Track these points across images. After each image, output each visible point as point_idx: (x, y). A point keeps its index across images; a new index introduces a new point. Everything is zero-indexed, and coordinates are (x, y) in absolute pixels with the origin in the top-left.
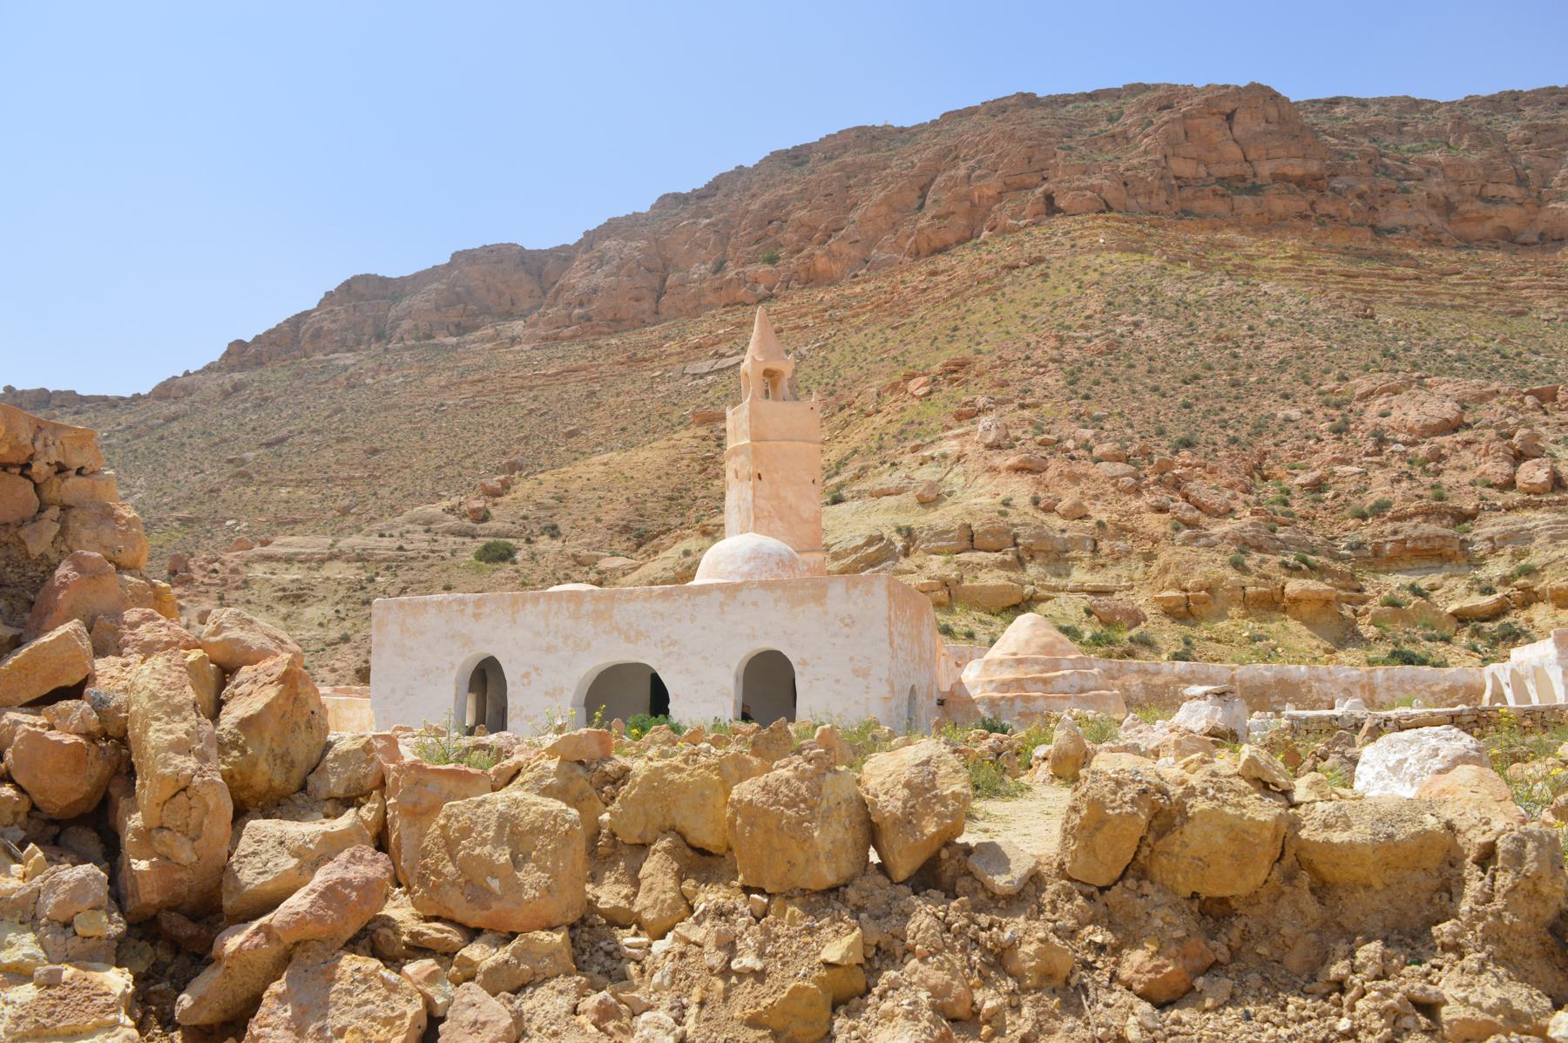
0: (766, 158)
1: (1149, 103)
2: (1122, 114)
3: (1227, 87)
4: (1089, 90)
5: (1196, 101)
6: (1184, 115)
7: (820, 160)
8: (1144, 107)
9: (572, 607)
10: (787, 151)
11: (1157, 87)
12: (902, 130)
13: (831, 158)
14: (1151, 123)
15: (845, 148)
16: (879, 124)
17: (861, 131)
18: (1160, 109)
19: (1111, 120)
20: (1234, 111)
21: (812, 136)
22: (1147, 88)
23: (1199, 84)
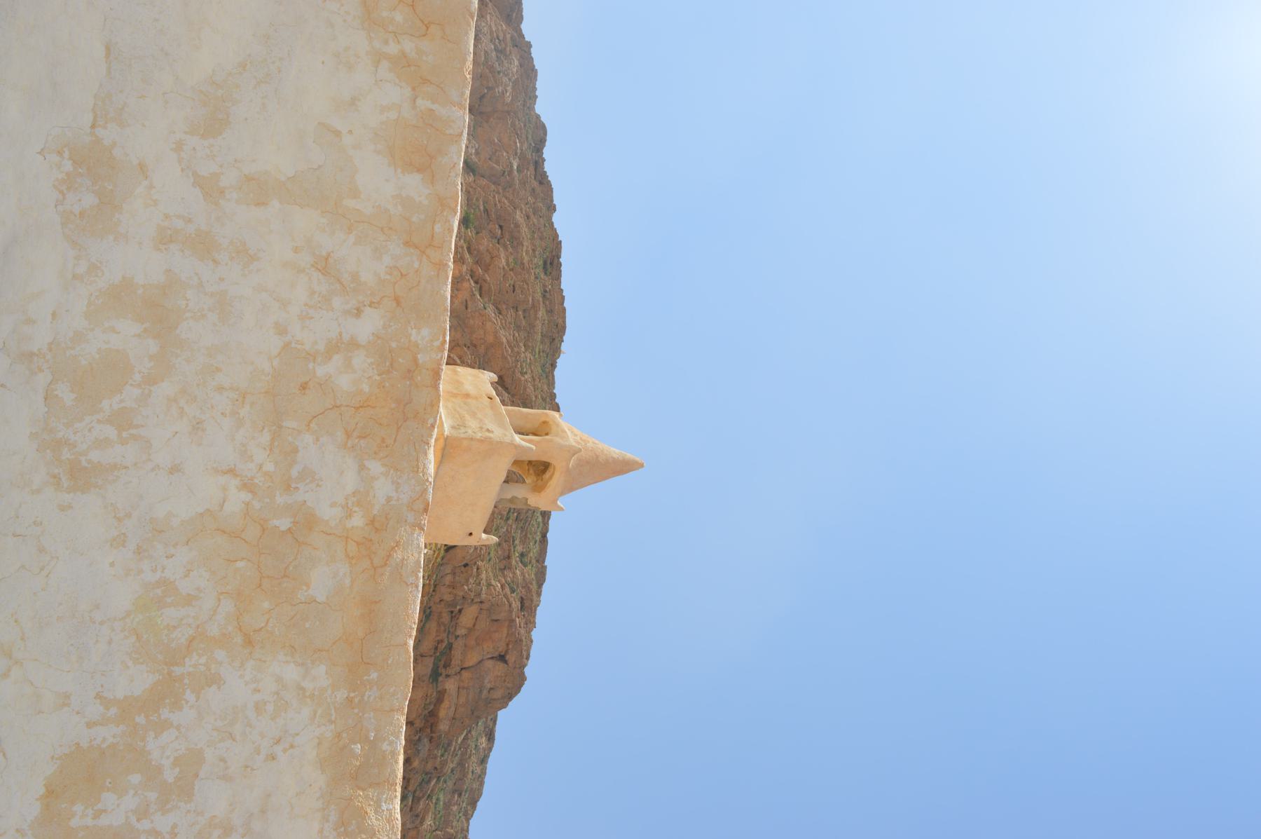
0: (557, 236)
1: (529, 590)
3: (528, 658)
5: (522, 631)
6: (513, 621)
7: (544, 286)
10: (559, 257)
11: (539, 594)
12: (553, 366)
13: (544, 296)
14: (513, 591)
15: (550, 312)
16: (564, 347)
17: (560, 329)
19: (522, 555)
22: (540, 585)
23: (534, 634)
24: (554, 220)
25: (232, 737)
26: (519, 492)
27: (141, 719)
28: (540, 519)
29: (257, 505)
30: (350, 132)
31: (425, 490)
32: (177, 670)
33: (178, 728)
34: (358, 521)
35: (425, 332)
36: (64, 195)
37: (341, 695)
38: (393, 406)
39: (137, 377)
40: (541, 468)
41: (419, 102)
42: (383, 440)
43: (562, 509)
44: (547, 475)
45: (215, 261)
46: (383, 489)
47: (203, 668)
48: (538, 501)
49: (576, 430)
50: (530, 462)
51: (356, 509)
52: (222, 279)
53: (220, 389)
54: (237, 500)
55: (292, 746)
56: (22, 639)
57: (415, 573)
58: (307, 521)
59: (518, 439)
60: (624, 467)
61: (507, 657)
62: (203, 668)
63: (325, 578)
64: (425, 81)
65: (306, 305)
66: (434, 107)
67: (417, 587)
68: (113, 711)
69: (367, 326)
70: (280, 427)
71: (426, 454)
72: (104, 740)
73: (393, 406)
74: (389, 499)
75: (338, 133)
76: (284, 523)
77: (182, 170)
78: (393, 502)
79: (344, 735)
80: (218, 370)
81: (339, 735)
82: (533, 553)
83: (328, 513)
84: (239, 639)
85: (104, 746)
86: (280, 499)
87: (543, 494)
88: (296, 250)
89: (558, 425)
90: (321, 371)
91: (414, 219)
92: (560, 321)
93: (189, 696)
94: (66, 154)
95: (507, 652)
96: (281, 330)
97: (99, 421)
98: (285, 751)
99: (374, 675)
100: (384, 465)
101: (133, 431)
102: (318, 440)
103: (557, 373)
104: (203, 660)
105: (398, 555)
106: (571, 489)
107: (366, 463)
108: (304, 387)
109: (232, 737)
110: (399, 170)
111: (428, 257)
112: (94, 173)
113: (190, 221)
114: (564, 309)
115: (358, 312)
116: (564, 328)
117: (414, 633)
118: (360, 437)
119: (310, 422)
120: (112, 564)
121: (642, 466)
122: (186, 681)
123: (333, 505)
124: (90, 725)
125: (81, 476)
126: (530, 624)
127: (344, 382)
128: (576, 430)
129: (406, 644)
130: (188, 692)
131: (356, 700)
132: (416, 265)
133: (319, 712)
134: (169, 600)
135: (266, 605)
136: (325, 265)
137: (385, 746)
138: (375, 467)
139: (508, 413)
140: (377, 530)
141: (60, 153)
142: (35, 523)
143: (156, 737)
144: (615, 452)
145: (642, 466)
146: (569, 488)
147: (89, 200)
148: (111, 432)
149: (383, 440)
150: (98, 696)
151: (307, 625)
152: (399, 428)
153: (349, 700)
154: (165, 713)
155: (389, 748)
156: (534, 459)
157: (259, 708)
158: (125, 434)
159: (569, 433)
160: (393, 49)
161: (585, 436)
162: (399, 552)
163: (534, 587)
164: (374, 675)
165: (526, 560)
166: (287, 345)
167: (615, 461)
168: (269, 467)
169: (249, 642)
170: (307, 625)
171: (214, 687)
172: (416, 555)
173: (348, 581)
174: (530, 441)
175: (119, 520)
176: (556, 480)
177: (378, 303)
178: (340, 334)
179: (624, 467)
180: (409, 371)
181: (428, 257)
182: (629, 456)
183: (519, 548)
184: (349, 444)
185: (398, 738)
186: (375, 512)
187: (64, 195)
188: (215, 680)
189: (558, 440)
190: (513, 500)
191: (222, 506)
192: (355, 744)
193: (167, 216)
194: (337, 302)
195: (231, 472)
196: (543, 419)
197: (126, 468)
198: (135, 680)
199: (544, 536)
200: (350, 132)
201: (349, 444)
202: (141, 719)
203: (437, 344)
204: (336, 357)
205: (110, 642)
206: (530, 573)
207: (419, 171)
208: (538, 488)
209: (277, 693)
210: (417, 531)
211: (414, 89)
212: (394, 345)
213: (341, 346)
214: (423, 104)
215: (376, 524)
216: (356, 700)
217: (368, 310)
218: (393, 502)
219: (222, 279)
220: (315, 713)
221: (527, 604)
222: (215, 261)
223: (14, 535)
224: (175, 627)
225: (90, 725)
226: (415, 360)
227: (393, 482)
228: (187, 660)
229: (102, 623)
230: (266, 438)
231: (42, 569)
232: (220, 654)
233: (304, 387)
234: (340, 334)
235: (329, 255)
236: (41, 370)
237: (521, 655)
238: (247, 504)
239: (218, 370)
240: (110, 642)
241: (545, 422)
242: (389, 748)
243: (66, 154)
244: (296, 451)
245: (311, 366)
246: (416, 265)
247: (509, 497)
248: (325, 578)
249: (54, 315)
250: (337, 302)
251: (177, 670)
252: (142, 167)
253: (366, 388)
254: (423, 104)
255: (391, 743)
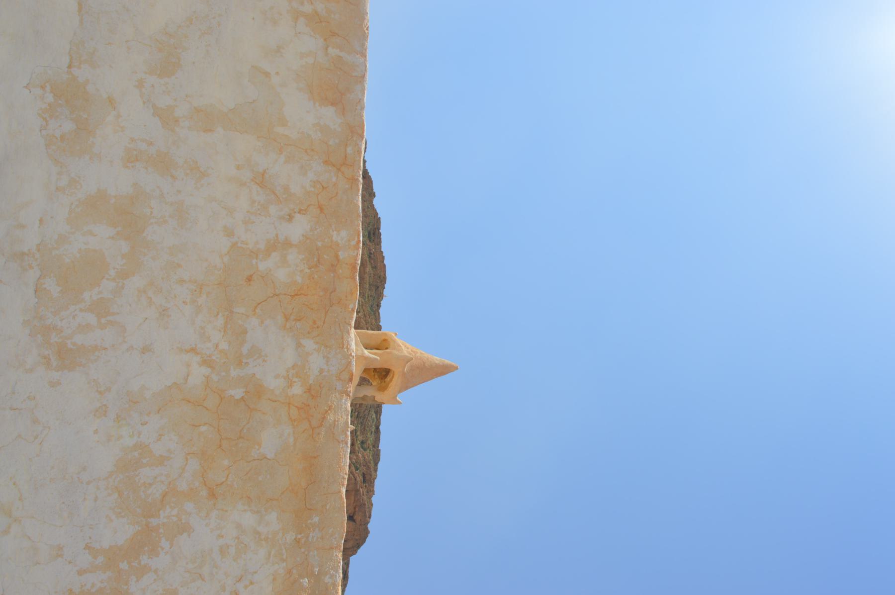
0: (377, 214)
1: (369, 468)
2: (365, 450)
3: (370, 517)
4: (381, 427)
5: (365, 498)
6: (358, 490)
7: (370, 250)
8: (366, 465)
9: (287, 270)
10: (379, 229)
11: (376, 470)
12: (379, 306)
13: (370, 257)
14: (357, 469)
15: (375, 268)
16: (385, 292)
17: (383, 280)
18: (364, 475)
19: (362, 443)
20: (354, 521)
21: (385, 246)
22: (376, 464)
23: (374, 499)
24: (374, 202)
25: (201, 577)
26: (369, 391)
27: (124, 566)
28: (374, 416)
29: (215, 378)
30: (277, 73)
31: (350, 363)
32: (154, 522)
33: (156, 571)
34: (297, 389)
35: (344, 233)
36: (46, 121)
37: (290, 537)
38: (321, 294)
39: (112, 273)
40: (384, 374)
41: (330, 50)
42: (315, 322)
43: (400, 403)
44: (388, 379)
45: (173, 177)
46: (316, 362)
47: (175, 519)
48: (379, 397)
49: (408, 345)
50: (375, 370)
51: (295, 379)
52: (179, 192)
53: (182, 281)
54: (199, 373)
55: (252, 583)
56: (20, 499)
57: (344, 432)
58: (256, 391)
59: (366, 352)
60: (443, 370)
61: (355, 517)
62: (175, 519)
63: (273, 438)
64: (334, 34)
65: (248, 212)
66: (342, 54)
67: (346, 443)
68: (100, 559)
69: (298, 229)
70: (232, 312)
71: (349, 333)
72: (93, 585)
73: (321, 294)
74: (321, 371)
75: (267, 74)
76: (238, 393)
77: (144, 103)
78: (325, 373)
79: (294, 571)
80: (179, 266)
81: (290, 572)
82: (370, 441)
83: (273, 383)
84: (204, 493)
85: (93, 590)
86: (234, 373)
87: (386, 392)
88: (238, 168)
89: (394, 341)
90: (262, 266)
91: (331, 143)
92: (382, 274)
93: (165, 544)
94: (48, 88)
95: (354, 513)
96: (229, 232)
97: (81, 310)
98: (246, 587)
99: (316, 519)
100: (317, 343)
101: (110, 318)
102: (262, 322)
103: (381, 311)
104: (175, 512)
105: (331, 417)
106: (407, 388)
107: (303, 342)
108: (249, 279)
109: (201, 577)
110: (317, 104)
111: (343, 173)
112: (71, 104)
113: (151, 144)
114: (385, 266)
115: (290, 218)
116: (385, 278)
117: (346, 483)
118: (296, 320)
119: (256, 308)
120: (96, 432)
121: (457, 368)
122: (161, 530)
123: (277, 377)
124: (81, 573)
125: (67, 357)
126: (370, 492)
127: (281, 275)
128: (408, 345)
129: (340, 492)
130: (163, 540)
131: (303, 541)
132: (334, 179)
133: (273, 553)
134: (145, 461)
135: (226, 463)
136: (262, 180)
137: (327, 579)
138: (309, 344)
139: (358, 334)
140: (313, 397)
141: (43, 88)
142: (29, 398)
143: (138, 581)
144: (437, 359)
145: (457, 368)
146: (405, 387)
147: (68, 126)
148: (91, 319)
149: (315, 322)
150: (87, 547)
151: (260, 479)
152: (327, 312)
153: (297, 541)
154: (145, 559)
155: (330, 581)
156: (379, 367)
157: (223, 550)
158: (103, 321)
159: (403, 347)
160: (307, 8)
161: (415, 349)
162: (332, 415)
163: (372, 465)
164: (316, 519)
165: (365, 446)
166: (234, 245)
167: (437, 366)
168: (224, 346)
169: (212, 495)
170: (260, 479)
171: (185, 534)
172: (345, 417)
173: (291, 440)
174: (375, 354)
175: (100, 393)
176: (395, 381)
177: (306, 210)
178: (277, 235)
179: (443, 370)
180: (332, 265)
181: (343, 173)
182: (447, 362)
183: (360, 438)
184: (288, 327)
185: (337, 571)
186: (311, 382)
187: (46, 121)
188: (185, 529)
189: (395, 352)
190: (364, 398)
191: (186, 379)
192: (303, 578)
193: (132, 140)
194: (273, 209)
195: (193, 350)
196: (383, 338)
197: (105, 349)
198: (118, 532)
199: (377, 428)
200: (277, 73)
201: (288, 327)
202: (124, 566)
203: (353, 243)
204: (274, 254)
205: (96, 499)
206: (369, 455)
207: (333, 104)
208: (382, 389)
209: (238, 538)
210: (345, 397)
211: (325, 40)
212: (320, 244)
213: (278, 245)
214: (333, 51)
215: (313, 392)
216: (303, 541)
217: (298, 216)
218: (325, 373)
219: (179, 192)
220: (269, 555)
221: (367, 477)
222: (173, 177)
223: (12, 409)
224: (151, 485)
225: (81, 573)
226: (337, 256)
227: (324, 357)
228: (161, 512)
229: (88, 483)
230: (220, 321)
231: (36, 438)
232: (189, 506)
233: (249, 279)
234: (277, 235)
235: (265, 171)
236: (31, 267)
237: (365, 516)
238: (207, 377)
239: (179, 266)
240: (96, 499)
241: (385, 340)
242: (330, 581)
243: (48, 88)
244: (245, 332)
245: (254, 261)
246: (334, 179)
247: (361, 396)
248: (273, 438)
249: (41, 221)
250: (273, 209)
251: (154, 522)
252: (111, 101)
253: (299, 279)
254: (333, 51)
255: (332, 576)
